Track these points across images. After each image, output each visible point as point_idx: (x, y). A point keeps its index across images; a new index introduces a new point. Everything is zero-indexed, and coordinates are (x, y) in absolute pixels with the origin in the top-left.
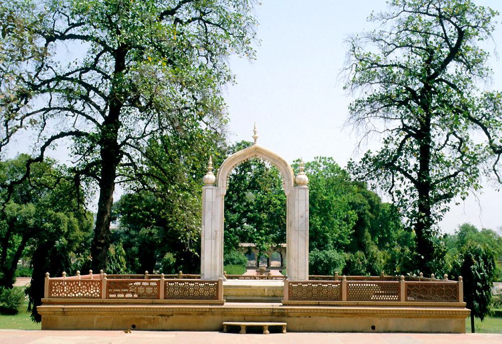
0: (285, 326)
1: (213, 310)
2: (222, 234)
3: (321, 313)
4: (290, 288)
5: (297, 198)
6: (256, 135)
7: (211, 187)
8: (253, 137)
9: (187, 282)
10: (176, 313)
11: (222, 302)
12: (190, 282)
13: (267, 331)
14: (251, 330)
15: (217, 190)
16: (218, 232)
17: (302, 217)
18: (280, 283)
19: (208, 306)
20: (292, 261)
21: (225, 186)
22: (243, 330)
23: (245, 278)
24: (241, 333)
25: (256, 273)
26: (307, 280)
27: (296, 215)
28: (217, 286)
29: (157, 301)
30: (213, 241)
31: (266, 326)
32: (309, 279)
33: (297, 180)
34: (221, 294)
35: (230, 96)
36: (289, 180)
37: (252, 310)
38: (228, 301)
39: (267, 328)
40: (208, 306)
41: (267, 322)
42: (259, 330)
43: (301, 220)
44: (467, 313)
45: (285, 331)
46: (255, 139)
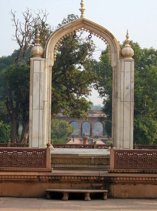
0: (106, 192)
1: (41, 178)
2: (49, 104)
3: (146, 181)
4: (116, 156)
5: (123, 70)
6: (83, 8)
7: (40, 58)
8: (80, 10)
9: (15, 150)
10: (5, 180)
11: (50, 170)
12: (18, 150)
13: (89, 198)
14: (74, 197)
15: (45, 62)
16: (46, 102)
17: (127, 88)
18: (104, 152)
19: (37, 174)
20: (118, 132)
21: (53, 58)
22: (66, 197)
23: (71, 146)
24: (63, 200)
25: (79, 141)
26: (132, 149)
27: (122, 88)
28: (45, 155)
29: (44, 169)
30: (41, 111)
31: (87, 193)
32: (133, 149)
33: (123, 53)
34: (49, 161)
35: (148, 48)
36: (116, 52)
37: (76, 178)
38: (55, 168)
39: (88, 195)
40: (37, 174)
41: (65, 189)
42: (80, 197)
43: (127, 92)
44: (41, 143)
45: (106, 197)
46: (82, 11)
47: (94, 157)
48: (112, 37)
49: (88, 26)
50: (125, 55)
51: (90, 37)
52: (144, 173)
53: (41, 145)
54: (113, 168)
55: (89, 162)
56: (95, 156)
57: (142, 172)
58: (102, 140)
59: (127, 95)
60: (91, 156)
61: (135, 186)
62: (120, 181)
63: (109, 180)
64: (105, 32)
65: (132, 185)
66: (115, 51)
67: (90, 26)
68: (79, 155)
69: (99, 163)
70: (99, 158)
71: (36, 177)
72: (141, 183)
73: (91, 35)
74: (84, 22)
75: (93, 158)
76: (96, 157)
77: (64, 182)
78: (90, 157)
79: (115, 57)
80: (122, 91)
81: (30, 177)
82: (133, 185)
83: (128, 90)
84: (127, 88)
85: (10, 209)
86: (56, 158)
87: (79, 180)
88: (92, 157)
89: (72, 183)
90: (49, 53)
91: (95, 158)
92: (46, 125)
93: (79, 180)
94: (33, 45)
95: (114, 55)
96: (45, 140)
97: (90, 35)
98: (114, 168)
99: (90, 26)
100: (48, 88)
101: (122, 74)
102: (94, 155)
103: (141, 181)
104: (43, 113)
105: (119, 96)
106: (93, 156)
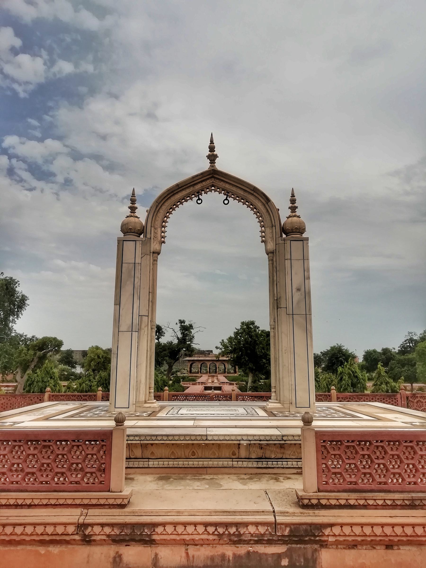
5: (289, 257)
37: (201, 529)
47: (249, 442)
48: (268, 200)
49: (222, 183)
50: (290, 231)
51: (226, 202)
52: (412, 506)
53: (134, 403)
54: (316, 489)
55: (234, 452)
56: (250, 438)
57: (407, 502)
58: (226, 377)
59: (298, 302)
60: (239, 438)
61: (390, 551)
62: (341, 539)
63: (306, 536)
64: (252, 192)
65: (381, 551)
66: (273, 225)
67: (227, 182)
68: (209, 438)
69: (260, 455)
70: (259, 444)
71: (71, 529)
72: (409, 543)
73: (228, 198)
74: (215, 176)
75: (245, 443)
76: (252, 442)
77: (164, 542)
78: (238, 442)
79: (273, 235)
80: (289, 294)
81: (55, 530)
82: (384, 547)
83: (299, 293)
84: (298, 290)
85: (184, 411)
86: (152, 444)
87: (211, 537)
88: (242, 442)
89: (188, 545)
90: (153, 228)
91: (250, 444)
92: (145, 363)
93: (211, 537)
94: (290, 496)
95: (271, 231)
96: (141, 392)
97: (226, 199)
98: (319, 491)
99: (227, 182)
100: (151, 291)
101: (288, 263)
102: (247, 435)
103: (411, 536)
104: (139, 338)
105: (283, 305)
106: (245, 438)
